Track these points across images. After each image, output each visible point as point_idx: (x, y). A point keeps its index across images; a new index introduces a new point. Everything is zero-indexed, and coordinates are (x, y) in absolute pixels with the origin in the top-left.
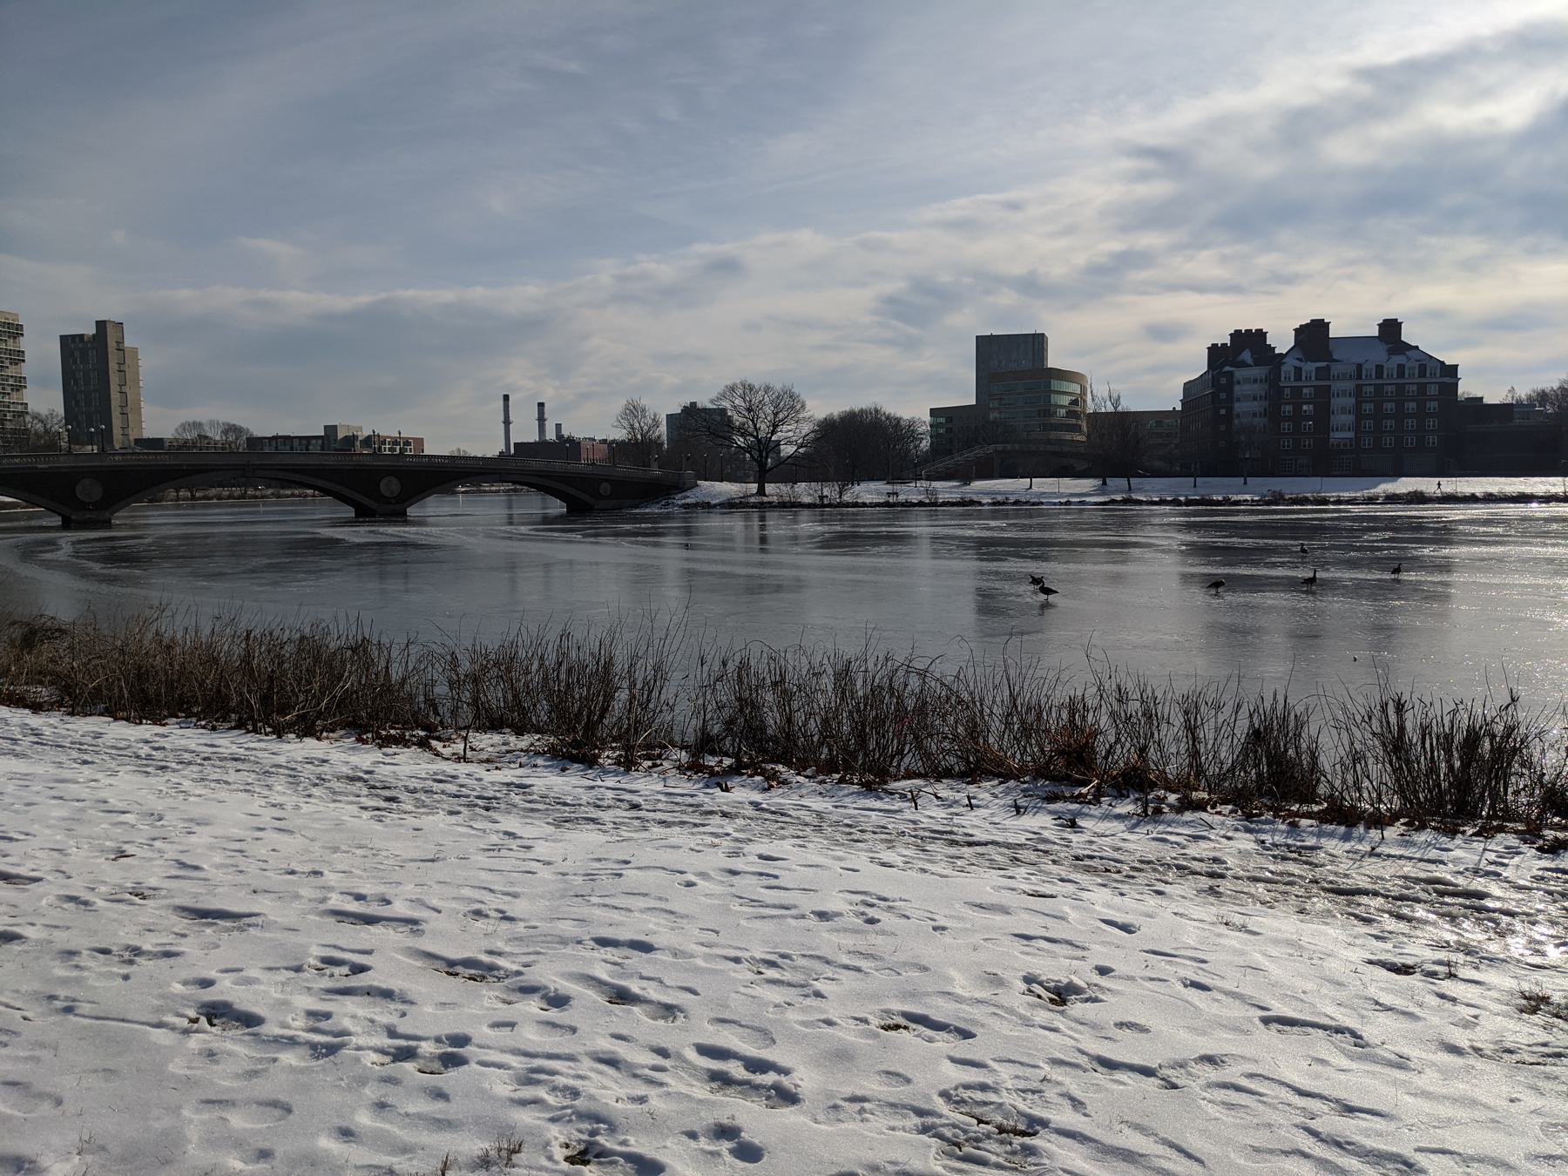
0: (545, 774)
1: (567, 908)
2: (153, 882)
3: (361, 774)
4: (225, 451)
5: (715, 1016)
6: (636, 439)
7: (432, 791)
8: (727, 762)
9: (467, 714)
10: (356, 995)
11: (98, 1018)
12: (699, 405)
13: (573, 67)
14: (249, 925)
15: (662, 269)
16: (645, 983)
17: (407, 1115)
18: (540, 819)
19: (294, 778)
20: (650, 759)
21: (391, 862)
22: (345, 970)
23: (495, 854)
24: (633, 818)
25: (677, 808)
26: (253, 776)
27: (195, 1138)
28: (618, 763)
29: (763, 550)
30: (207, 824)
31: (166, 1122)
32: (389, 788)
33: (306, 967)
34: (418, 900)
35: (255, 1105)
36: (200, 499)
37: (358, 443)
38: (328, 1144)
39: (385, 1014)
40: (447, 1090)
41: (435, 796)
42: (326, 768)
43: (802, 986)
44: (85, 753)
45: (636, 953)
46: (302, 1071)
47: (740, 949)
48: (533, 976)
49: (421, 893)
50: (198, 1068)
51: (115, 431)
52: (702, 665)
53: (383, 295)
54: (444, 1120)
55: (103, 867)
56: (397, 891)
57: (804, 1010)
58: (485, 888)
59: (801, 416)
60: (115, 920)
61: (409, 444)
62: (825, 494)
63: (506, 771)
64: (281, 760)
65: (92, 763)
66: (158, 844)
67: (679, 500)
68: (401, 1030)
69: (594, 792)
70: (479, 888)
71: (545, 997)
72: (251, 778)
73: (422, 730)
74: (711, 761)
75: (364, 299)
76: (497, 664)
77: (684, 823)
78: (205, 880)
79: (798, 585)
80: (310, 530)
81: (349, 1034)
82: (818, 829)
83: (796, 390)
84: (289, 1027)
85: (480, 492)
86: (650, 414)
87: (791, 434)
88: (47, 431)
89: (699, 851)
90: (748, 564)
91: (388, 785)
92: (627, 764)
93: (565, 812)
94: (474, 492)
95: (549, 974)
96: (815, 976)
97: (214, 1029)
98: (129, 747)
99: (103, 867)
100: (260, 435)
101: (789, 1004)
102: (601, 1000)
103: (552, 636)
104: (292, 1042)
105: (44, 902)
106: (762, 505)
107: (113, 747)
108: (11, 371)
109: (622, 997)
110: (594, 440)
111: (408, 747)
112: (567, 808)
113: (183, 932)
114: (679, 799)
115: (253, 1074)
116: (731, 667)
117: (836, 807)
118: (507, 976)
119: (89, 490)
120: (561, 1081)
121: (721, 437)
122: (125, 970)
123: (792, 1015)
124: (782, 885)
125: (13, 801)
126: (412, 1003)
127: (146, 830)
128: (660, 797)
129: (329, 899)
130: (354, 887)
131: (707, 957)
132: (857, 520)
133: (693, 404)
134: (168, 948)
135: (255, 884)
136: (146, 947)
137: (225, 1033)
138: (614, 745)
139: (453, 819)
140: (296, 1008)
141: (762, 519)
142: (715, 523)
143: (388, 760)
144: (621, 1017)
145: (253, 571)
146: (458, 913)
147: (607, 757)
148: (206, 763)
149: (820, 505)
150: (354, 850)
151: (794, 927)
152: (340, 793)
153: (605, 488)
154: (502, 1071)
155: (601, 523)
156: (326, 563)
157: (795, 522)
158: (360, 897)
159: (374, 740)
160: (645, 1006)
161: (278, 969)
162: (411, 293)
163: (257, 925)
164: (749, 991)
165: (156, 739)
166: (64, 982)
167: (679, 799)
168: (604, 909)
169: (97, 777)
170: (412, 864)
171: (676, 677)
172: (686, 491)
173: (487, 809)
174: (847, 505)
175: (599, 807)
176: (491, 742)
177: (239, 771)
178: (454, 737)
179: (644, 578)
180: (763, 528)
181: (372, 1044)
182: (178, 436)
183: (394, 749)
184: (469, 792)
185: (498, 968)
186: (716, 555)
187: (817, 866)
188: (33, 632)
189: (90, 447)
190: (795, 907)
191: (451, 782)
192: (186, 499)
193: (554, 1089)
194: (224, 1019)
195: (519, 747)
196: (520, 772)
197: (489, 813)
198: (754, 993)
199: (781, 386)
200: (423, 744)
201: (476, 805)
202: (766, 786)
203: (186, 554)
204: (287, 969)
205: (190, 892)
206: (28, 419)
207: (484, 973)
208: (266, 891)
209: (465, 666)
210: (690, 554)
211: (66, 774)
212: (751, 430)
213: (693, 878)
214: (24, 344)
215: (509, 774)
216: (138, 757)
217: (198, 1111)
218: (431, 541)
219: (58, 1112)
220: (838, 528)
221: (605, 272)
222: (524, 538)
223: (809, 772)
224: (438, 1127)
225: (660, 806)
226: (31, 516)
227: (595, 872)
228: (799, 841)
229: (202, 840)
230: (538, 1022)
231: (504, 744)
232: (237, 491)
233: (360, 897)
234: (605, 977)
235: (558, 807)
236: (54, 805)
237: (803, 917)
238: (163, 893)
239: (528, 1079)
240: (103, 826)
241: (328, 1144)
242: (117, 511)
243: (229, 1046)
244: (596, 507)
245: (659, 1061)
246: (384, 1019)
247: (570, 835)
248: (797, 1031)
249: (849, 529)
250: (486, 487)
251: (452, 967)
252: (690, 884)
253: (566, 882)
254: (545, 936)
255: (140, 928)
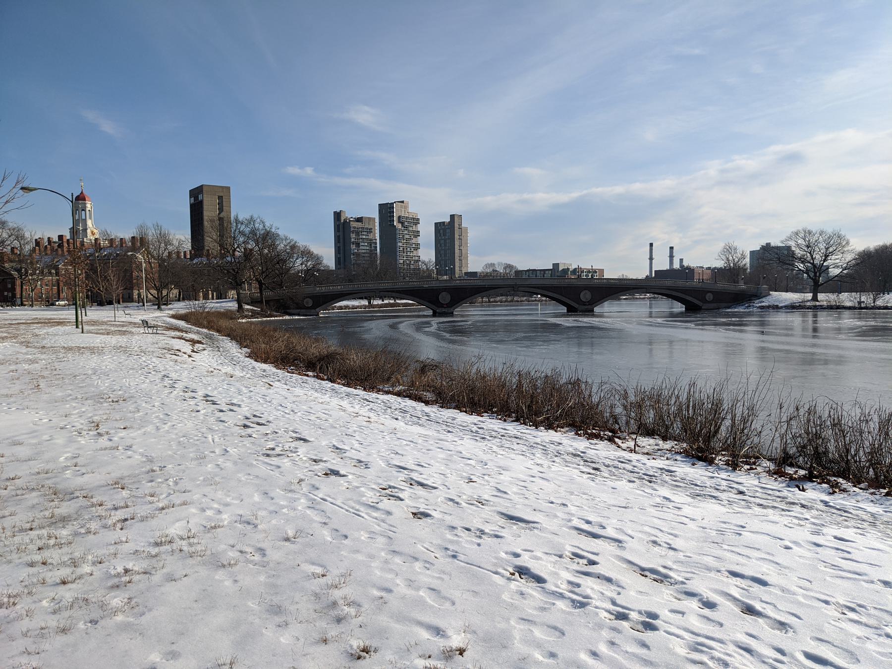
0: (683, 466)
1: (709, 549)
2: (486, 497)
3: (579, 453)
4: (504, 277)
5: (814, 635)
6: (730, 267)
7: (618, 467)
8: (802, 472)
9: (634, 426)
10: (592, 577)
11: (468, 564)
12: (773, 244)
13: (697, 51)
14: (534, 528)
15: (748, 163)
16: (764, 605)
17: (627, 652)
18: (682, 492)
19: (545, 451)
20: (748, 464)
21: (602, 505)
22: (585, 561)
23: (660, 509)
24: (740, 500)
25: (769, 497)
26: (525, 447)
27: (518, 638)
28: (727, 464)
29: (814, 337)
30: (508, 470)
31: (502, 625)
32: (595, 462)
33: (564, 556)
34: (620, 529)
35: (545, 627)
36: (492, 302)
37: (569, 273)
38: (584, 657)
39: (610, 591)
40: (648, 642)
41: (620, 470)
42: (561, 447)
43: (876, 628)
44: (449, 428)
45: (756, 585)
46: (569, 613)
47: (828, 595)
48: (692, 586)
49: (621, 525)
50: (516, 600)
51: (456, 269)
52: (781, 409)
53: (585, 192)
54: (649, 661)
55: (463, 485)
56: (608, 522)
57: (879, 644)
58: (657, 529)
59: (846, 249)
60: (471, 514)
61: (596, 272)
62: (862, 300)
63: (658, 461)
64: (538, 440)
65: (452, 432)
66: (486, 477)
67: (757, 303)
68: (618, 602)
69: (714, 480)
70: (654, 528)
71: (700, 600)
72: (525, 448)
73: (610, 432)
74: (790, 470)
75: (575, 195)
76: (650, 398)
77: (775, 507)
78: (510, 500)
79: (840, 361)
80: (544, 319)
81: (591, 598)
82: (873, 524)
83: (843, 233)
84: (559, 588)
85: (634, 298)
86: (739, 252)
87: (838, 261)
88: (427, 269)
89: (790, 528)
90: (804, 345)
91: (594, 461)
92: (734, 466)
93: (697, 490)
94: (630, 299)
95: (702, 586)
96: (884, 623)
97: (522, 580)
98: (468, 426)
99: (463, 485)
100: (521, 269)
101: (868, 638)
102: (737, 610)
103: (684, 383)
104: (562, 596)
105: (439, 500)
106: (815, 308)
107: (461, 425)
108: (414, 241)
109: (750, 610)
110: (703, 268)
111: (603, 441)
112: (698, 488)
113: (503, 525)
114: (770, 492)
115: (543, 609)
116: (802, 412)
117: (886, 512)
118: (676, 583)
119: (445, 298)
120: (717, 654)
121: (787, 264)
122: (479, 541)
123: (870, 646)
124: (854, 558)
125: (422, 447)
126: (623, 588)
127: (480, 470)
128: (757, 489)
129: (573, 520)
130: (585, 516)
131: (805, 597)
132: (887, 318)
133: (768, 244)
134: (497, 533)
135: (535, 506)
136: (487, 531)
137: (527, 584)
138: (723, 453)
139: (631, 485)
140: (562, 578)
141: (815, 316)
142: (781, 318)
143: (592, 447)
144: (750, 623)
145: (517, 340)
146: (643, 540)
147: (720, 460)
148: (503, 438)
149: (859, 308)
150: (581, 495)
151: (866, 588)
152: (569, 462)
153: (709, 297)
154: (679, 639)
155: (707, 317)
156: (553, 337)
157: (839, 318)
158: (588, 522)
159: (584, 435)
160: (766, 619)
161: (550, 554)
162: (600, 190)
163: (538, 529)
164: (837, 624)
165: (480, 423)
166: (451, 542)
167: (770, 492)
168: (732, 553)
169: (455, 440)
170: (614, 508)
171: (762, 416)
172: (761, 298)
173: (650, 482)
174: (880, 308)
175: (717, 489)
176: (649, 443)
177: (518, 444)
178: (627, 437)
179: (732, 352)
180: (815, 322)
181: (604, 607)
182: (484, 271)
183: (595, 441)
184: (639, 471)
185: (671, 578)
186: (784, 339)
187: (878, 550)
188: (425, 366)
189: (445, 277)
190: (866, 575)
191: (628, 464)
192: (486, 302)
193: (712, 658)
194: (526, 576)
195: (665, 447)
196: (667, 462)
197: (652, 484)
198: (841, 626)
199: (832, 230)
200: (611, 440)
201: (643, 479)
202: (831, 491)
203: (486, 330)
204: (555, 555)
205: (504, 506)
206: (420, 263)
207: (662, 579)
208: (540, 511)
209: (632, 398)
210: (765, 337)
211: (442, 436)
212: (808, 259)
213: (790, 545)
214: (420, 227)
215: (661, 463)
216: (472, 431)
217: (518, 623)
218: (607, 326)
219: (453, 608)
220: (873, 323)
221: (713, 168)
222: (660, 325)
223: (862, 486)
224: (645, 664)
225: (758, 494)
226: (420, 310)
227: (724, 530)
228: (859, 531)
229: (507, 479)
230: (698, 615)
231: (656, 445)
232: (509, 298)
233: (588, 522)
234: (737, 596)
235: (692, 486)
236: (439, 451)
237: (872, 582)
238: (492, 503)
239: (696, 648)
240: (461, 465)
241: (584, 657)
242: (456, 308)
243: (530, 591)
244: (703, 307)
245: (779, 656)
246: (609, 594)
247: (702, 504)
248: (875, 657)
249: (881, 324)
250: (637, 296)
251: (643, 571)
252: (787, 548)
253: (705, 532)
254: (697, 563)
255: (483, 520)
